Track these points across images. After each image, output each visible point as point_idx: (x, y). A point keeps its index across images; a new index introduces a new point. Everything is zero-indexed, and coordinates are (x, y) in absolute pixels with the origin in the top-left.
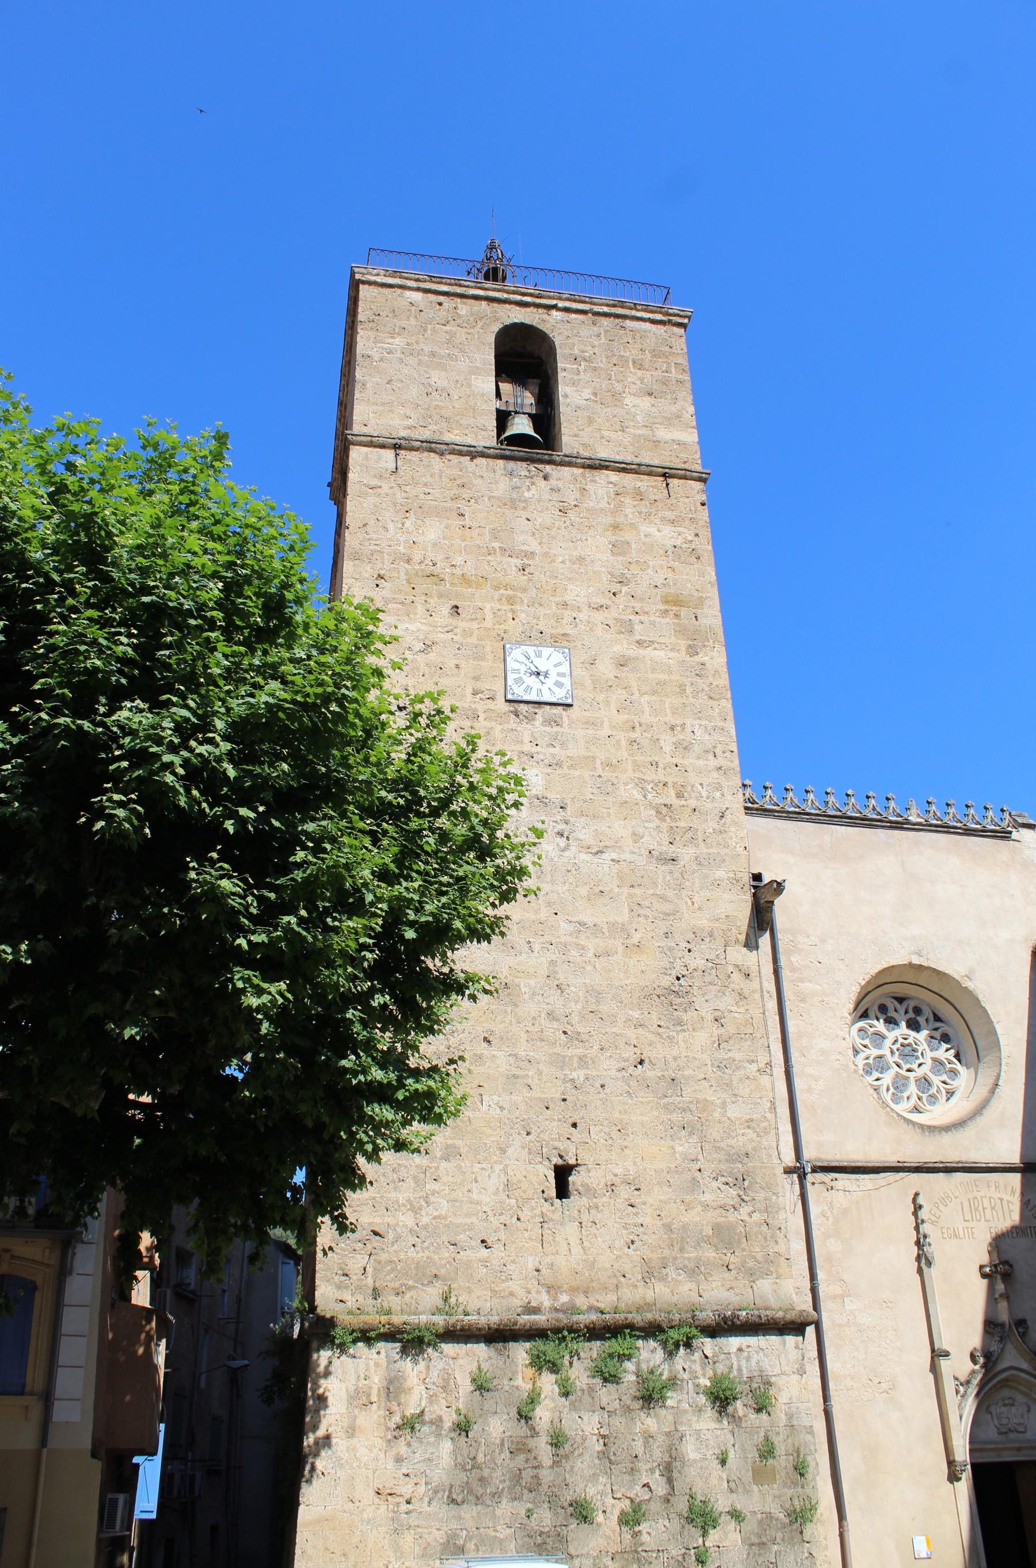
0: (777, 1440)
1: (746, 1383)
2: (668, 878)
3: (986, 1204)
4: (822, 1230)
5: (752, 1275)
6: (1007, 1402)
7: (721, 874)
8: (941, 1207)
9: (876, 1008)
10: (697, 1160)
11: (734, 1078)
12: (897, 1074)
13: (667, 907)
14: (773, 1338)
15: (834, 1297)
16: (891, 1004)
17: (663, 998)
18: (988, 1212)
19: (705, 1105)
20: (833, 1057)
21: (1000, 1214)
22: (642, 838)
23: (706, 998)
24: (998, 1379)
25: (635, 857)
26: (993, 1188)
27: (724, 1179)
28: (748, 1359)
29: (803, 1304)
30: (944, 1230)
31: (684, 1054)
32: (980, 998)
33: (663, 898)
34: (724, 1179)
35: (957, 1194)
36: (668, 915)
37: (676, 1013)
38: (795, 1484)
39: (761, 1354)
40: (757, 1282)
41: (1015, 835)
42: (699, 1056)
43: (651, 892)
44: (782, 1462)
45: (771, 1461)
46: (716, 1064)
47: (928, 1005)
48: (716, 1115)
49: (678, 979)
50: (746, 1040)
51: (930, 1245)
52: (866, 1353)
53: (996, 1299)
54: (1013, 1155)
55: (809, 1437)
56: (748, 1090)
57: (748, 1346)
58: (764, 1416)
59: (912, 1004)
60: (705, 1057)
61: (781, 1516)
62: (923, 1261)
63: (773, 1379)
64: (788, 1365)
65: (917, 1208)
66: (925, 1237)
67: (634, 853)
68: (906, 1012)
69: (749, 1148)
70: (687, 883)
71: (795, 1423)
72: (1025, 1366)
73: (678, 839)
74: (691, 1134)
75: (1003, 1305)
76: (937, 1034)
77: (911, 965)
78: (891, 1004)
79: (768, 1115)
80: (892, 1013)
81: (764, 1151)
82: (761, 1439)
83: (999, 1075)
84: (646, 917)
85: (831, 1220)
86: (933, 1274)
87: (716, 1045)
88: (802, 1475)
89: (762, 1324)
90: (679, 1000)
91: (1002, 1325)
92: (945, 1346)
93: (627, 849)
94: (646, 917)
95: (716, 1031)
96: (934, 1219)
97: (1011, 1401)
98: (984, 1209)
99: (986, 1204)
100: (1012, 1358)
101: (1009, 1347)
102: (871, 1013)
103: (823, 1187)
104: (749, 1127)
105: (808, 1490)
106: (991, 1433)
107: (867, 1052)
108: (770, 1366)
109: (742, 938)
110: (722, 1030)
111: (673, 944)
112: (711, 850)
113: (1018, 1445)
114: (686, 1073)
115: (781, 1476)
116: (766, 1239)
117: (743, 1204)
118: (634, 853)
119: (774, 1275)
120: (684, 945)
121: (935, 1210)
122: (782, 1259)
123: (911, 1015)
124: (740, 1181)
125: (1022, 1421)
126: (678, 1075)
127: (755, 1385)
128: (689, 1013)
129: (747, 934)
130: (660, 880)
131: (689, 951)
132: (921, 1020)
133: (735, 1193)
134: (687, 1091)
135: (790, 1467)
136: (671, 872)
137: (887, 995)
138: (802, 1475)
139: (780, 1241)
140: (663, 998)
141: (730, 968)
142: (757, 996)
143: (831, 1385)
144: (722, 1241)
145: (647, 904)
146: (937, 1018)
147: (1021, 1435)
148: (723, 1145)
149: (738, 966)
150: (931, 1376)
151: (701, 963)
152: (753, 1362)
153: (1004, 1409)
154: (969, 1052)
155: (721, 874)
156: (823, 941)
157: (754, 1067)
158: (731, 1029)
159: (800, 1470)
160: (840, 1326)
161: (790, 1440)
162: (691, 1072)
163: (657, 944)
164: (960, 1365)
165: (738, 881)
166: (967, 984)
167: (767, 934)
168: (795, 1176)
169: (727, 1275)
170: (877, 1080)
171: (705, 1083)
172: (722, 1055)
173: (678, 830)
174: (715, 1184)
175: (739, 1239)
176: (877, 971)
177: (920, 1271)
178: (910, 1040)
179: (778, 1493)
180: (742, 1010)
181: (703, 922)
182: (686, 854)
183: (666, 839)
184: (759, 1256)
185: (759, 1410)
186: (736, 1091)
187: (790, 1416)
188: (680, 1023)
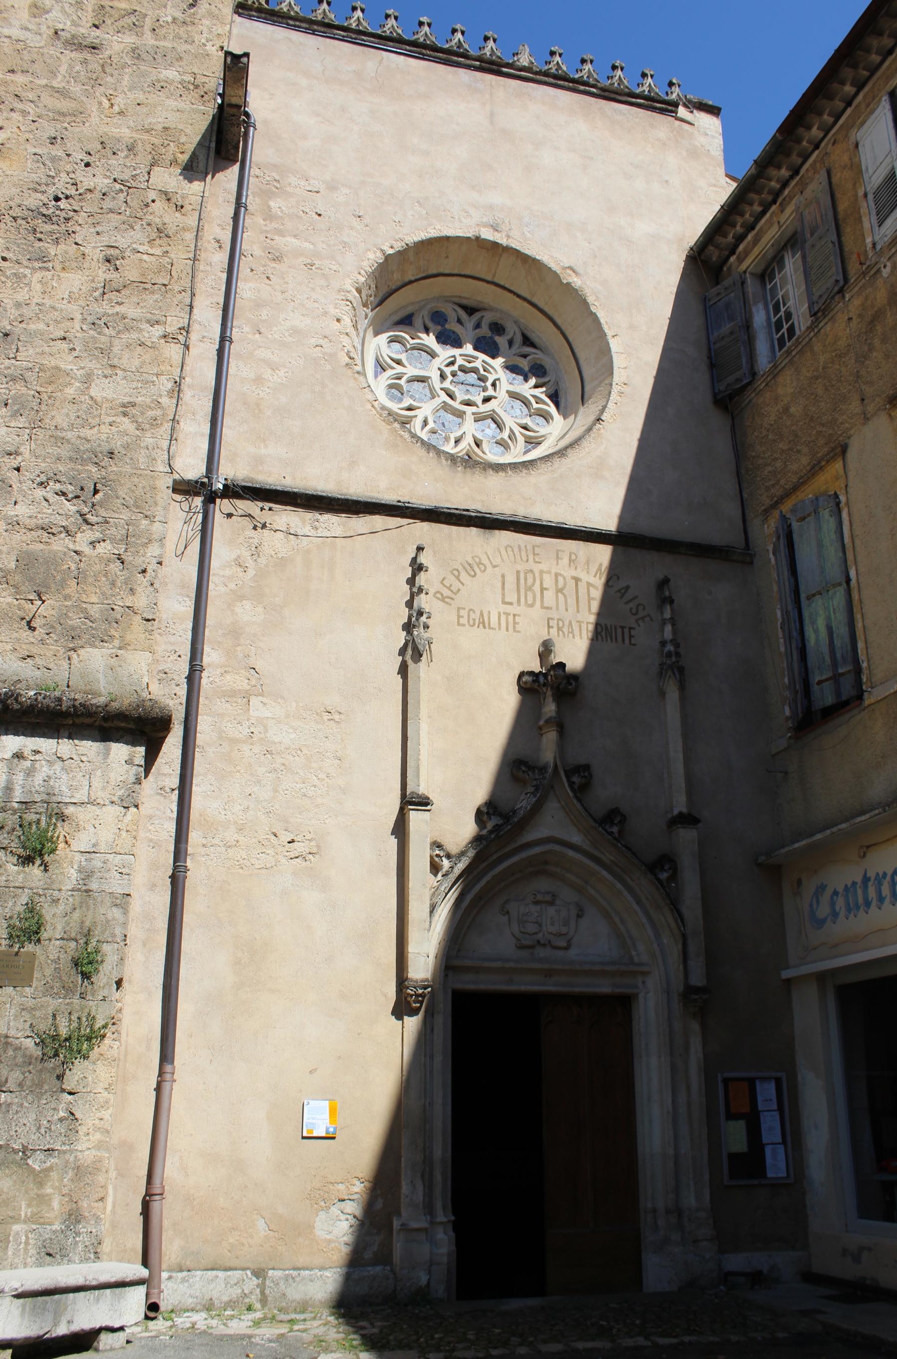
0: (48, 912)
1: (15, 812)
2: (78, 68)
3: (548, 581)
4: (232, 586)
5: (73, 640)
6: (539, 897)
7: (171, 74)
8: (464, 576)
9: (425, 313)
10: (17, 453)
11: (116, 342)
12: (445, 407)
13: (64, 105)
14: (88, 744)
15: (231, 695)
16: (452, 312)
17: (20, 221)
18: (550, 595)
19: (56, 375)
20: (313, 341)
21: (572, 601)
22: (47, 12)
23: (99, 229)
24: (524, 855)
25: (28, 35)
26: (566, 561)
27: (58, 486)
28: (30, 773)
29: (171, 697)
30: (464, 613)
31: (35, 301)
32: (590, 299)
33: (63, 93)
34: (58, 486)
35: (497, 561)
36: (64, 115)
37: (38, 244)
38: (68, 990)
39: (58, 765)
40: (81, 652)
41: (682, 111)
42: (64, 305)
43: (44, 82)
44: (52, 952)
45: (29, 947)
46: (90, 319)
47: (516, 322)
48: (70, 391)
49: (57, 199)
50: (153, 293)
51: (426, 627)
52: (276, 791)
53: (540, 728)
54: (605, 512)
55: (116, 913)
56: (137, 362)
57: (37, 752)
58: (35, 871)
59: (488, 317)
60: (74, 310)
61: (29, 1043)
62: (409, 651)
63: (70, 810)
64: (104, 788)
65: (417, 568)
66: (420, 613)
67: (27, 29)
68: (478, 326)
69: (117, 444)
70: (109, 79)
71: (94, 886)
72: (576, 838)
73: (109, 22)
74: (17, 414)
75: (551, 737)
76: (524, 364)
77: (479, 242)
78: (452, 312)
79: (165, 400)
80: (452, 326)
81: (143, 451)
82: (20, 908)
83: (604, 407)
84: (24, 113)
85: (251, 572)
86: (422, 671)
87: (97, 294)
88: (86, 976)
89: (65, 715)
90: (48, 227)
91: (543, 769)
92: (422, 790)
93: (17, 23)
94: (24, 113)
95: (102, 274)
96: (446, 592)
97: (548, 898)
98: (543, 589)
99: (548, 581)
100: (555, 824)
101: (552, 806)
102: (418, 321)
103: (247, 523)
104: (125, 414)
105: (91, 1004)
106: (498, 941)
107: (399, 369)
108: (70, 787)
109: (185, 157)
110: (114, 275)
111: (60, 153)
112: (162, 43)
113: (546, 966)
114: (33, 327)
115: (43, 973)
116: (113, 584)
117: (85, 527)
118: (27, 29)
119: (117, 643)
120: (79, 156)
121: (451, 580)
122: (139, 617)
123: (485, 331)
124: (89, 495)
125: (564, 930)
126: (18, 329)
127: (31, 817)
128: (62, 247)
129: (194, 153)
130: (63, 69)
131: (87, 165)
132: (501, 341)
133: (74, 509)
134: (28, 354)
135: (65, 960)
136: (85, 62)
137: (447, 300)
138: (86, 976)
139: (139, 590)
140: (20, 221)
141: (152, 195)
142: (190, 236)
143: (194, 836)
144: (31, 580)
145: (31, 96)
146: (527, 341)
147: (561, 953)
148: (69, 435)
149: (166, 193)
150: (393, 842)
151: (102, 182)
152: (38, 779)
153: (534, 909)
154: (572, 390)
155: (171, 74)
156: (332, 187)
157: (158, 331)
158: (131, 273)
159: (85, 966)
160: (233, 741)
161: (76, 915)
162: (41, 326)
163: (34, 150)
164: (453, 822)
165: (197, 87)
166: (570, 278)
167: (236, 167)
168: (198, 501)
169: (26, 634)
170: (409, 409)
171: (64, 346)
172: (105, 307)
173: (113, 12)
174: (40, 493)
175: (64, 580)
176: (417, 239)
177: (403, 670)
178: (478, 364)
179: (31, 1003)
180: (158, 251)
181: (123, 131)
182: (117, 43)
183: (88, 18)
184: (94, 611)
185: (27, 860)
186: (115, 362)
187: (87, 875)
188: (43, 258)
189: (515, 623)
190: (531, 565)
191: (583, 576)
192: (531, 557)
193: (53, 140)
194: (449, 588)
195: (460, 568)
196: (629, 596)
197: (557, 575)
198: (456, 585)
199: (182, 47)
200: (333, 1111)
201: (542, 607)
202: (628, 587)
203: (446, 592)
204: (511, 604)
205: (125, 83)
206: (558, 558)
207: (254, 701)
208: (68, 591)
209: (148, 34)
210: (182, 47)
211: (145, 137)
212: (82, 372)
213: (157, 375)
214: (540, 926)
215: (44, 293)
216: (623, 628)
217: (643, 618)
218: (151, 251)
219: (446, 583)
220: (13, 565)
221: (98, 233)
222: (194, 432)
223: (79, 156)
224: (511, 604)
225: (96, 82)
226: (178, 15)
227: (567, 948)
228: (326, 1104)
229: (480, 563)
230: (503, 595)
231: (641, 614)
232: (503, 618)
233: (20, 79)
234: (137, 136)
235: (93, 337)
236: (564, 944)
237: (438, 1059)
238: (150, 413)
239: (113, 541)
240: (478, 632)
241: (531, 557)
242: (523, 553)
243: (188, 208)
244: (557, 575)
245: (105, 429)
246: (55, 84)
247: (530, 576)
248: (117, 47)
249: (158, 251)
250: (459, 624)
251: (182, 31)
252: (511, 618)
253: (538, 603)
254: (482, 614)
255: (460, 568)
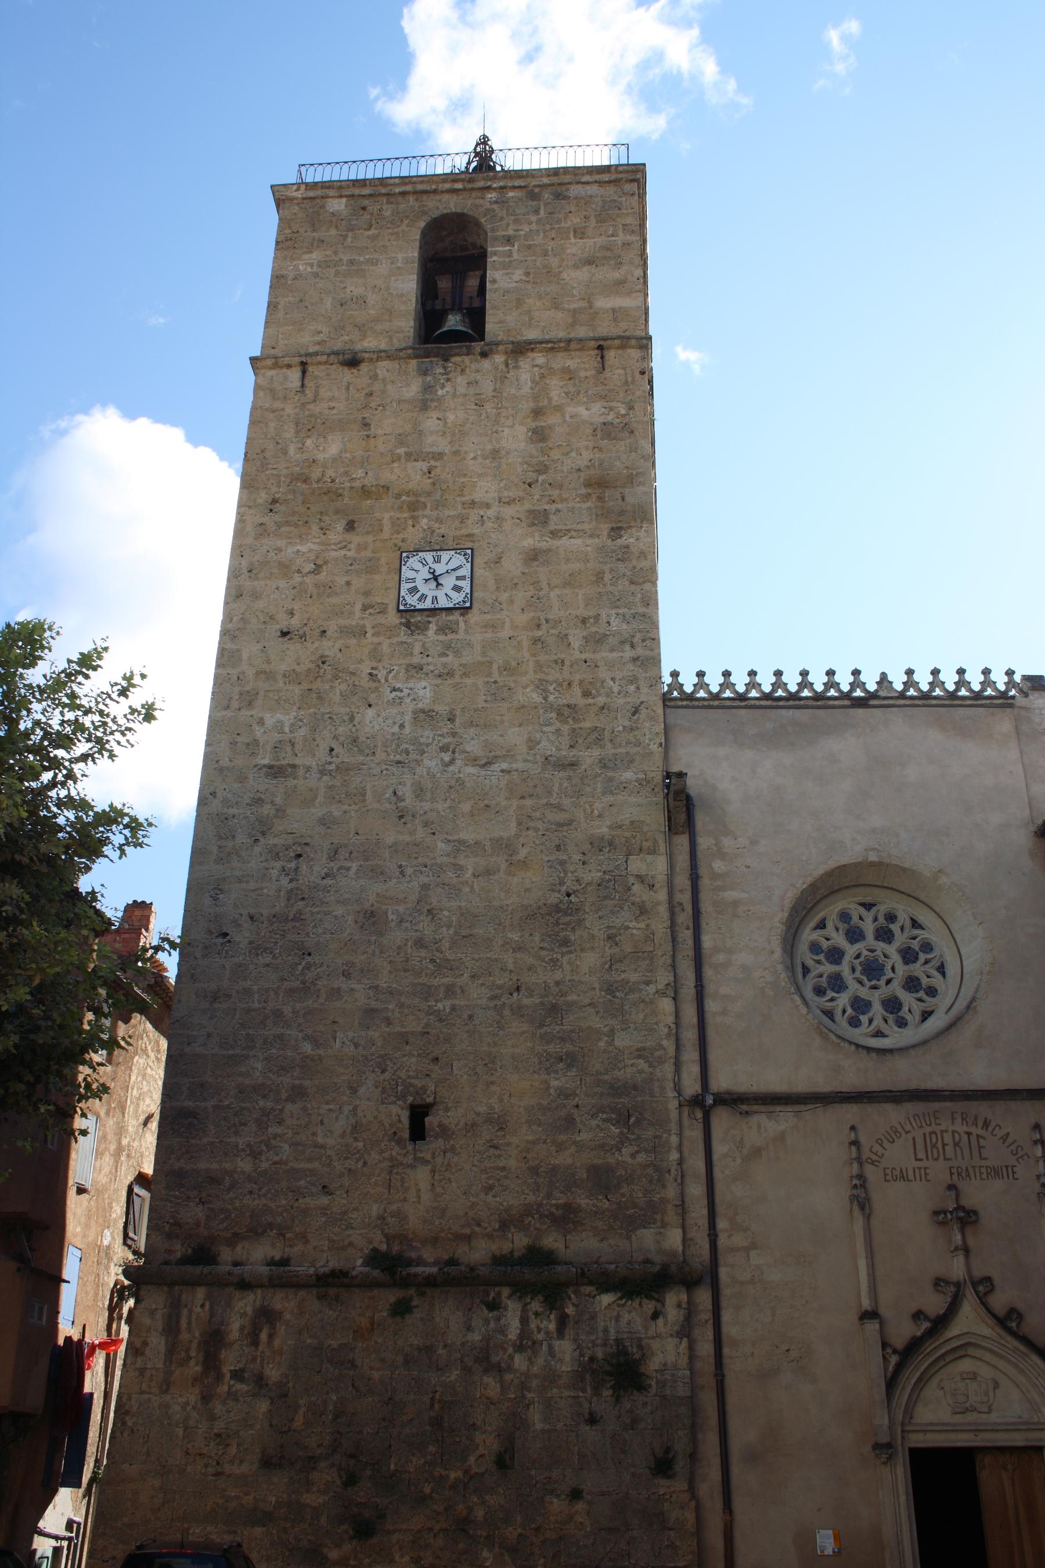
3: (948, 1138)
6: (965, 1376)
8: (886, 1144)
13: (561, 817)
18: (949, 1149)
21: (966, 1152)
25: (529, 765)
26: (959, 1120)
27: (605, 1116)
30: (888, 1171)
31: (568, 978)
33: (559, 808)
35: (908, 1127)
36: (562, 825)
40: (638, 1232)
43: (545, 801)
49: (569, 895)
68: (875, 919)
73: (580, 741)
79: (665, 1043)
84: (537, 830)
98: (944, 1145)
99: (948, 1138)
110: (616, 950)
121: (877, 1148)
125: (985, 1399)
130: (556, 788)
131: (584, 863)
136: (569, 778)
145: (538, 814)
147: (985, 1416)
155: (628, 775)
157: (651, 989)
163: (547, 859)
180: (642, 925)
182: (589, 757)
188: (566, 942)
189: (926, 1174)
190: (934, 1127)
191: (974, 1130)
192: (933, 1120)
193: (558, 848)
194: (876, 1154)
195: (882, 1137)
196: (1010, 1140)
197: (954, 1132)
198: (880, 1150)
199: (633, 750)
200: (837, 1537)
201: (945, 1159)
202: (1008, 1134)
203: (874, 1158)
204: (921, 1160)
205: (599, 790)
206: (953, 1119)
207: (752, 1253)
208: (622, 1191)
209: (609, 745)
210: (633, 750)
211: (619, 832)
212: (607, 1028)
213: (656, 1023)
214: (968, 1397)
215: (572, 971)
216: (1007, 1167)
217: (1021, 1157)
218: (638, 926)
219: (874, 1150)
220: (585, 1176)
221: (600, 918)
222: (692, 1070)
223: (577, 857)
224: (921, 1160)
225: (579, 794)
226: (627, 723)
227: (989, 1412)
228: (830, 1532)
229: (896, 1132)
230: (915, 1153)
231: (1020, 1153)
232: (917, 1171)
233: (528, 802)
234: (614, 833)
235: (610, 1001)
236: (986, 1410)
237: (903, 1498)
238: (657, 1053)
239: (646, 1151)
240: (901, 1184)
241: (933, 1120)
242: (927, 1118)
243: (657, 885)
244: (954, 1132)
245: (629, 1070)
246: (552, 801)
247: (933, 1136)
248: (589, 761)
249: (642, 925)
250: (886, 1180)
251: (631, 737)
252: (923, 1171)
253: (942, 1157)
254: (901, 1171)
255: (882, 1137)
